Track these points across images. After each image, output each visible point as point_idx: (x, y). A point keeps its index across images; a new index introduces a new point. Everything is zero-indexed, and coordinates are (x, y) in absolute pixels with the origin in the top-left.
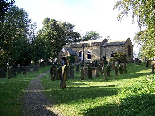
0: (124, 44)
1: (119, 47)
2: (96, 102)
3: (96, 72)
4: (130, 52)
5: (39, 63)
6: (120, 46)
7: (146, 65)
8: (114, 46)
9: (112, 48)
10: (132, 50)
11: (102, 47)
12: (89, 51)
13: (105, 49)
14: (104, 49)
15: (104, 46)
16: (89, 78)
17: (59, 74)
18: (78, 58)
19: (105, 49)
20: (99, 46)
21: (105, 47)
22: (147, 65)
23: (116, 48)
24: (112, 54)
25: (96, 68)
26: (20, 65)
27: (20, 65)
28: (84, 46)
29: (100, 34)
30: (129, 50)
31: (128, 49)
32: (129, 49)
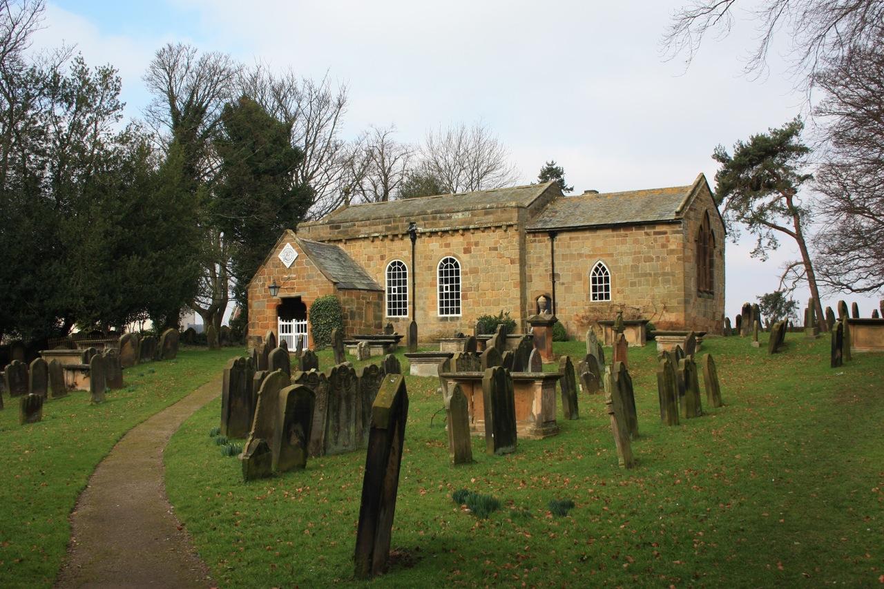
0: (672, 217)
1: (640, 234)
2: (328, 460)
3: (536, 408)
4: (712, 264)
5: (129, 336)
6: (651, 231)
7: (833, 353)
8: (609, 232)
9: (599, 243)
10: (722, 253)
11: (529, 237)
12: (400, 263)
13: (553, 252)
14: (540, 248)
15: (543, 231)
16: (501, 450)
17: (299, 427)
18: (379, 307)
19: (553, 252)
20: (511, 232)
21: (553, 234)
22: (839, 353)
23: (623, 243)
24: (594, 280)
25: (539, 378)
26: (4, 335)
27: (4, 335)
28: (420, 229)
29: (767, 124)
30: (705, 253)
31: (698, 247)
32: (705, 249)
